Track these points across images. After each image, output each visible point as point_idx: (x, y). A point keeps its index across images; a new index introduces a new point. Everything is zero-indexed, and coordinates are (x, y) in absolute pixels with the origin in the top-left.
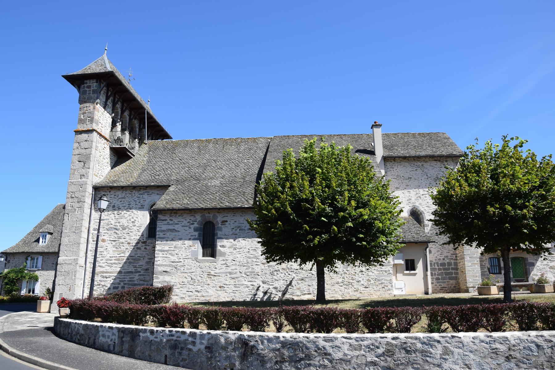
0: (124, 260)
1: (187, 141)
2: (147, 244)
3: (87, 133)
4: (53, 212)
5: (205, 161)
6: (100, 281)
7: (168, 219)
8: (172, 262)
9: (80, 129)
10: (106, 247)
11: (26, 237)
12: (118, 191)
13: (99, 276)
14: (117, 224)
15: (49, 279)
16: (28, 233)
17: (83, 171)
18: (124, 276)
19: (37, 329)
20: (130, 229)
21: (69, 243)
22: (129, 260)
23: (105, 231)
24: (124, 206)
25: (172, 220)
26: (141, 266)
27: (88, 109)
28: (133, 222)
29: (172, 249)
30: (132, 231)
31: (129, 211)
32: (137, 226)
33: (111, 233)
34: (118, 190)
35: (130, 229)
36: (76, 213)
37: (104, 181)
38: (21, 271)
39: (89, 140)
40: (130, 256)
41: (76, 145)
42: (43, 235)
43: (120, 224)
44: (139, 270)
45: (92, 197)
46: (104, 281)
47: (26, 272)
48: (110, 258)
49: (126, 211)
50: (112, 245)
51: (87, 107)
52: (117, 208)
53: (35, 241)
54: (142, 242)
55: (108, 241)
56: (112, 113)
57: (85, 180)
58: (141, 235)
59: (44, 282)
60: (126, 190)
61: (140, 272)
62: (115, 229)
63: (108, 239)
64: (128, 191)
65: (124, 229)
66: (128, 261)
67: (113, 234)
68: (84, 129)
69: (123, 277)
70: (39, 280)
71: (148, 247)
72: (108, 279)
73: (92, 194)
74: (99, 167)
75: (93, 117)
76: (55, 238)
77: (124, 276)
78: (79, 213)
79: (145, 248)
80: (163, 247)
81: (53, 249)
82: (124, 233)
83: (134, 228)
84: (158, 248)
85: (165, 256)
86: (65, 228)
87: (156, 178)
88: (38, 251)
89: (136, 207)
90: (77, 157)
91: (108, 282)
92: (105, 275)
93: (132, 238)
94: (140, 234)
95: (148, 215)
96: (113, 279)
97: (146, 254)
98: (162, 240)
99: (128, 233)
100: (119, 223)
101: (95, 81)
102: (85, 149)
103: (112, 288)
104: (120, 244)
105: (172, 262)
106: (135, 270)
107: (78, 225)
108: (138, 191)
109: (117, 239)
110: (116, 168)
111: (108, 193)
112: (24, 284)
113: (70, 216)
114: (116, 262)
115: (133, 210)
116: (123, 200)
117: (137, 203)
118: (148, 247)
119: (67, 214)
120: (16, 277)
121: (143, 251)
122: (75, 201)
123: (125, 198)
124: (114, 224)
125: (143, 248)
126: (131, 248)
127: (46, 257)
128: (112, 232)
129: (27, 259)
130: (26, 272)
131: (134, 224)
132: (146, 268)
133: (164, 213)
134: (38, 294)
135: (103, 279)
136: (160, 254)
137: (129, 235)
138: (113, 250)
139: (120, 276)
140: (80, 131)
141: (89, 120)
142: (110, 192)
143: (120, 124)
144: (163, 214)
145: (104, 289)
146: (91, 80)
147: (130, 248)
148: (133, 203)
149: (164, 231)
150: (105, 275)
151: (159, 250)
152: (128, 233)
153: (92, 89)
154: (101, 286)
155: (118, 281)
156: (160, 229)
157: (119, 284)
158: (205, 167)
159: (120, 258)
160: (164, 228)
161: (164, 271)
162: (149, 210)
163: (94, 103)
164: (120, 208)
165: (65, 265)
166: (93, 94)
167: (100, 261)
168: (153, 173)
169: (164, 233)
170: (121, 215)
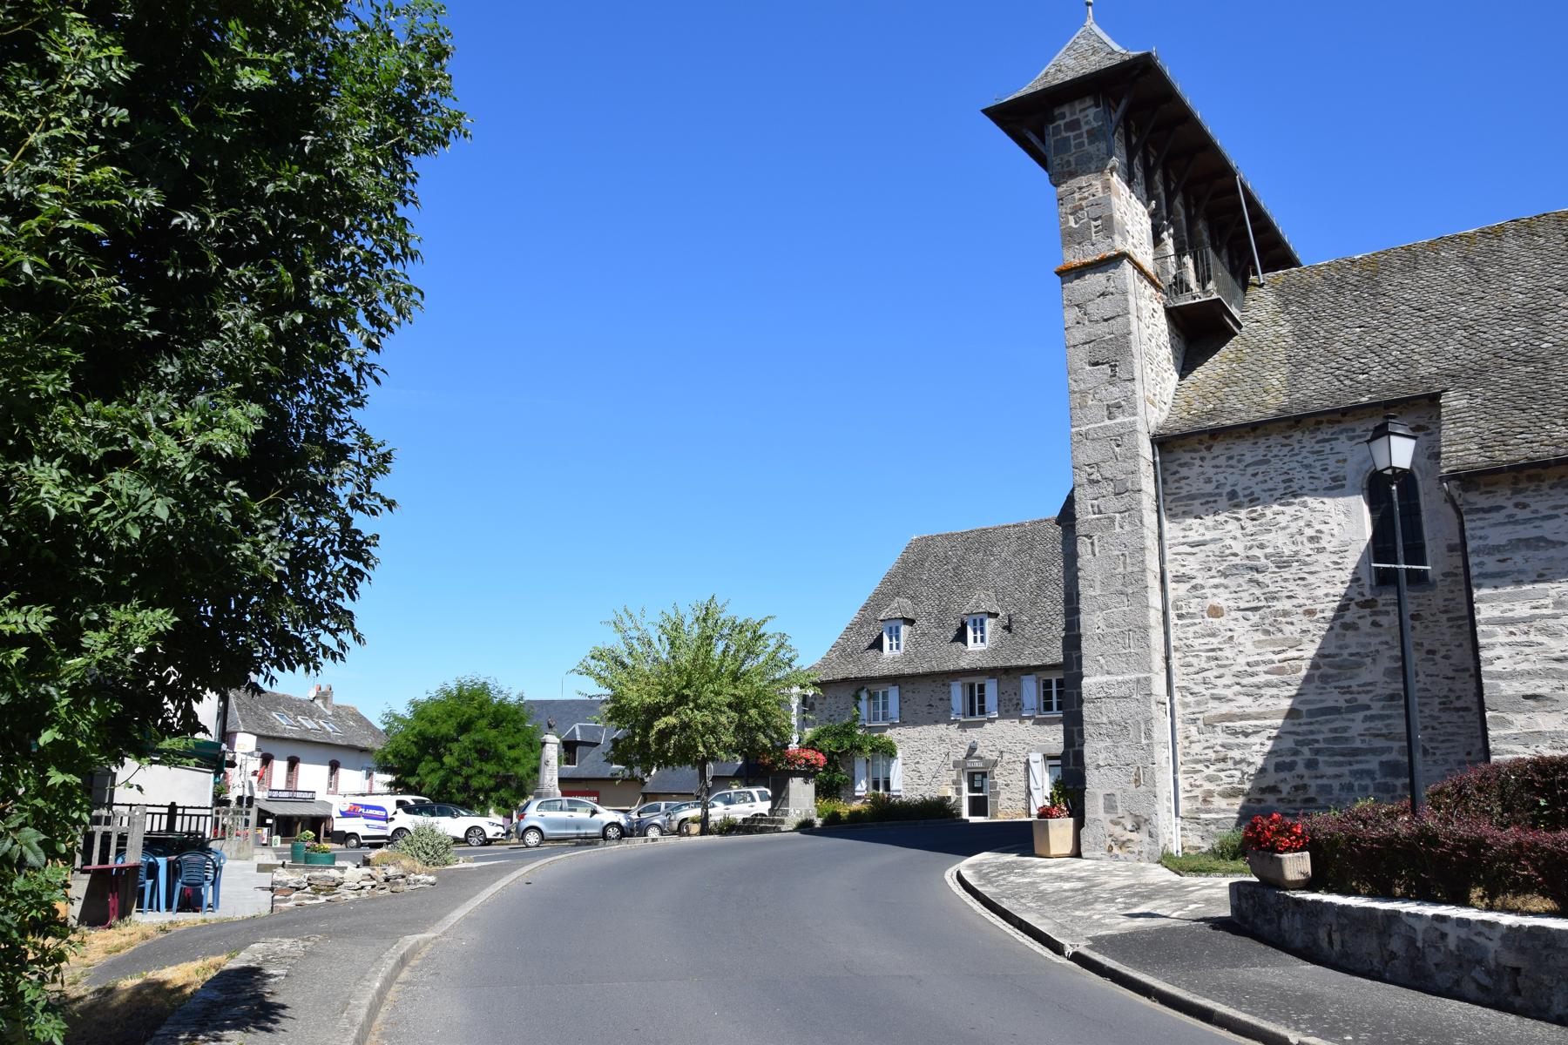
0: (1299, 669)
1: (1408, 249)
2: (1380, 608)
3: (1101, 269)
4: (904, 561)
5: (1521, 296)
6: (1223, 746)
7: (1510, 504)
8: (1558, 660)
9: (1076, 262)
10: (1230, 634)
11: (845, 637)
12: (1237, 442)
13: (1219, 730)
14: (1257, 552)
15: (925, 749)
16: (847, 625)
17: (1115, 393)
18: (1311, 723)
19: (1163, 930)
20: (1306, 564)
21: (1110, 630)
22: (1321, 670)
23: (1216, 581)
24: (1270, 490)
25: (1525, 506)
26: (1369, 688)
27: (1086, 194)
28: (1311, 539)
29: (1544, 611)
30: (1313, 569)
31: (1293, 503)
32: (1330, 548)
33: (1240, 585)
34: (1237, 438)
35: (1306, 564)
36: (1118, 530)
37: (1174, 418)
38: (847, 731)
39: (1111, 290)
40: (1321, 655)
41: (1071, 315)
42: (891, 628)
43: (1267, 551)
44: (1363, 699)
45: (1155, 472)
46: (1238, 746)
47: (859, 732)
48: (1247, 668)
49: (1281, 505)
50: (1247, 624)
51: (1080, 188)
52: (1247, 499)
53: (871, 647)
54: (1357, 604)
55: (1233, 613)
56: (1149, 200)
57: (1126, 420)
58: (1352, 581)
59: (912, 757)
60: (1267, 435)
61: (1368, 707)
62: (1251, 568)
63: (1232, 604)
64: (1274, 436)
65: (1283, 564)
66: (1317, 673)
67: (1245, 587)
68: (1089, 259)
69: (1305, 728)
70: (899, 754)
71: (1383, 620)
72: (1251, 740)
73: (1154, 463)
74: (1153, 375)
75: (1111, 217)
76: (924, 634)
77: (1311, 723)
78: (1127, 528)
79: (1375, 624)
80: (1507, 606)
81: (925, 666)
82: (1286, 580)
83: (1320, 557)
84: (1484, 612)
85: (1522, 638)
86: (1087, 583)
87: (1358, 382)
88: (886, 672)
89: (1313, 487)
90: (1082, 352)
91: (1257, 747)
92: (1238, 724)
93: (1320, 593)
94: (1347, 575)
95: (1366, 508)
96: (1269, 738)
97: (1382, 643)
98: (1497, 581)
99: (1303, 579)
100: (1262, 546)
101: (1089, 102)
102: (1106, 320)
103: (1271, 768)
104: (1279, 619)
105: (1558, 660)
106: (1346, 701)
107: (1129, 569)
108: (1312, 432)
109: (1263, 603)
110: (1195, 373)
111: (1204, 453)
112: (860, 766)
113: (1096, 542)
114: (1274, 678)
115: (1306, 498)
116: (1263, 468)
117: (1317, 472)
118: (1383, 620)
119: (1086, 536)
120: (838, 748)
121: (1369, 635)
122: (1105, 493)
123: (1267, 462)
124: (1242, 553)
125: (1365, 625)
126: (1320, 629)
127: (910, 687)
128: (1241, 580)
129: (857, 698)
130: (859, 732)
131: (1317, 545)
132: (1388, 692)
133: (1486, 485)
134: (899, 791)
135: (1232, 740)
136: (1501, 635)
137: (1305, 586)
138: (1256, 639)
139: (1294, 725)
140: (1076, 268)
141: (1096, 227)
142: (1209, 448)
143: (1169, 235)
144: (1483, 489)
145: (1243, 774)
146: (1077, 103)
147: (1319, 630)
148: (1301, 477)
149: (1498, 548)
150: (1238, 724)
151: (1489, 622)
152: (1303, 579)
153: (1085, 128)
154: (1230, 764)
155: (1289, 742)
156: (1481, 542)
157: (1296, 753)
158: (1534, 316)
159: (1285, 664)
160: (1498, 536)
161: (1526, 697)
162: (1363, 489)
163: (1102, 172)
164: (1256, 495)
165: (1108, 700)
166: (1091, 143)
167: (1213, 680)
168: (1338, 369)
169: (1500, 557)
170: (1263, 520)
